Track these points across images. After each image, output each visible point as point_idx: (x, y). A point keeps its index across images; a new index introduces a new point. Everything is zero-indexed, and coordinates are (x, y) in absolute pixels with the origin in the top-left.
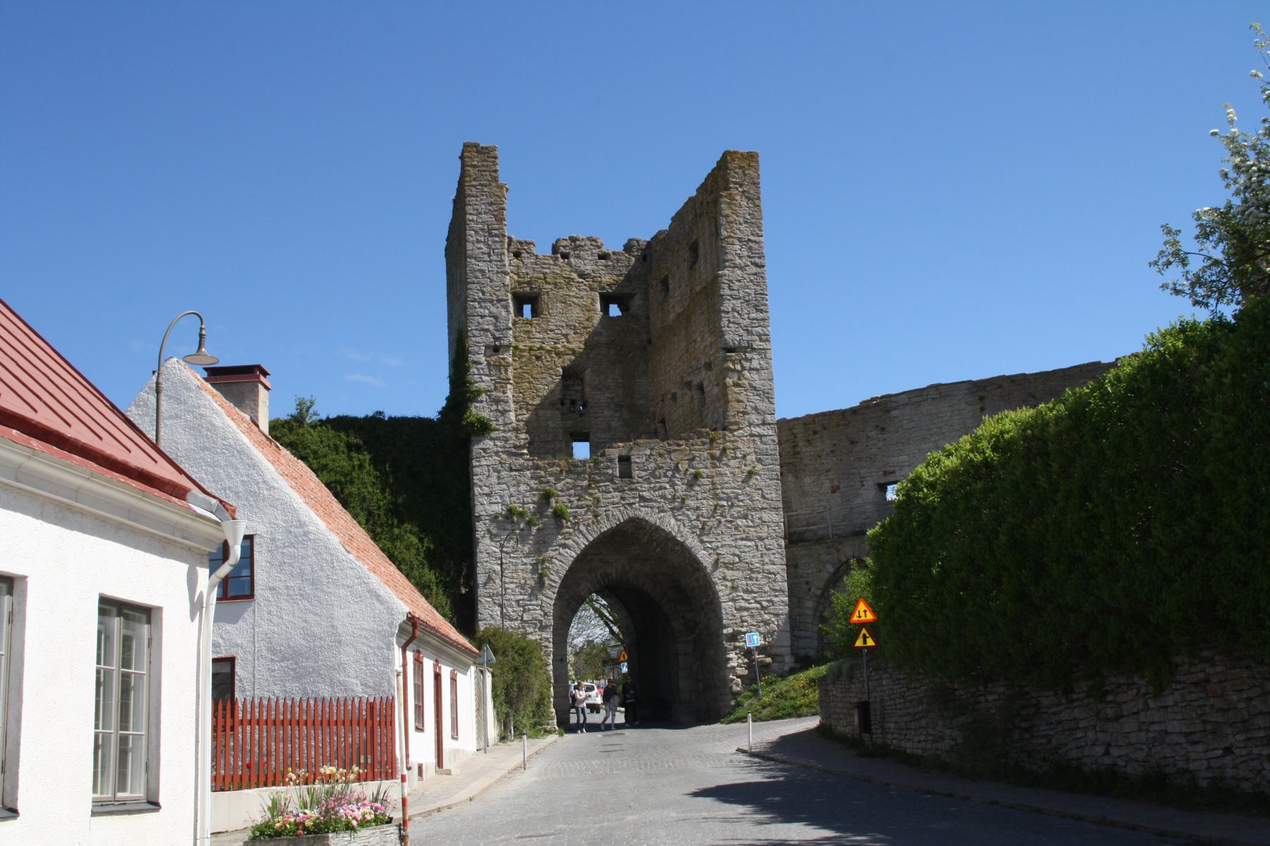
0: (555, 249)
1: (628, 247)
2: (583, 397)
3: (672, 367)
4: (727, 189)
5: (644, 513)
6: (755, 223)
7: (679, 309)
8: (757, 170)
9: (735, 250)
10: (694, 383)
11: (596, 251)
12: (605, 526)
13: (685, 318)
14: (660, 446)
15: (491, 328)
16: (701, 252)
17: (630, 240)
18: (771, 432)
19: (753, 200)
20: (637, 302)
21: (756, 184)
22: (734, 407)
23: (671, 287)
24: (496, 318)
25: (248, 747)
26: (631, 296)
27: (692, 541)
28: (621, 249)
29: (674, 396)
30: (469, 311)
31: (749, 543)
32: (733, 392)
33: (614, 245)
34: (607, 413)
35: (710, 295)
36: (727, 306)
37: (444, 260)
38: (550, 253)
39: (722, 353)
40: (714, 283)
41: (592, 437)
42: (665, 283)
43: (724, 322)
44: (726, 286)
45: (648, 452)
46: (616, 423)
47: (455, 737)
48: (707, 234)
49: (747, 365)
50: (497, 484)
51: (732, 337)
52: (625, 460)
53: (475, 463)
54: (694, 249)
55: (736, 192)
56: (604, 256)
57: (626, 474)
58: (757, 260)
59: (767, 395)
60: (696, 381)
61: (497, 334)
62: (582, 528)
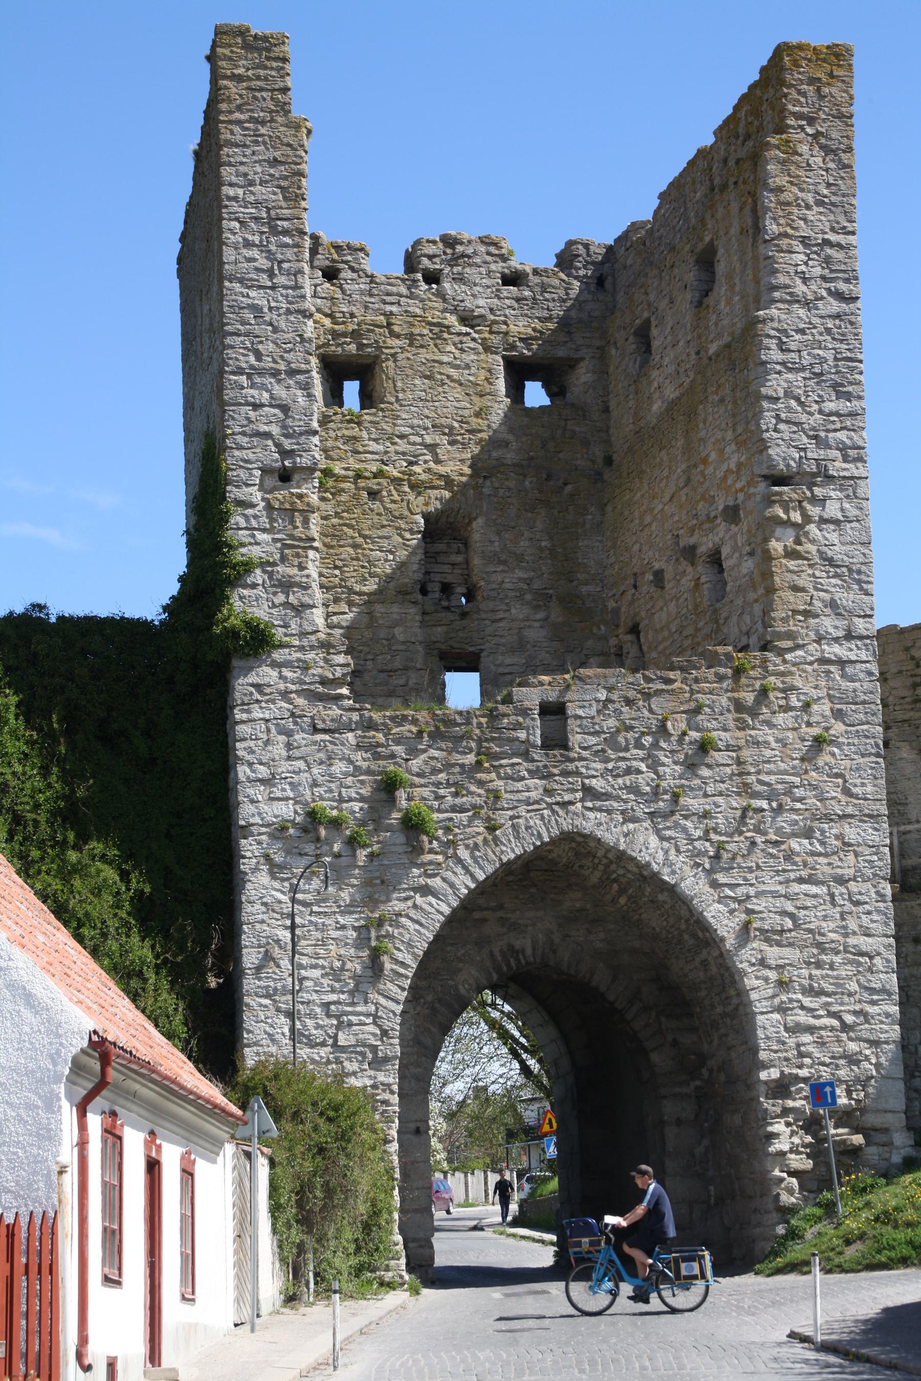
0: (411, 262)
1: (565, 260)
2: (466, 578)
4: (781, 129)
5: (608, 830)
7: (671, 393)
8: (848, 84)
9: (794, 264)
12: (511, 850)
13: (685, 410)
14: (625, 681)
15: (275, 430)
16: (721, 268)
17: (570, 243)
19: (838, 153)
21: (845, 118)
22: (786, 601)
26: (572, 364)
28: (550, 262)
29: (659, 576)
31: (814, 890)
32: (784, 571)
33: (535, 253)
34: (518, 611)
35: (737, 362)
36: (775, 385)
40: (748, 336)
42: (643, 336)
44: (773, 344)
45: (602, 695)
46: (536, 634)
49: (814, 511)
50: (285, 759)
51: (782, 452)
52: (554, 711)
54: (706, 261)
56: (513, 279)
57: (556, 741)
58: (842, 287)
59: (858, 577)
60: (706, 545)
61: (287, 444)
62: (463, 853)
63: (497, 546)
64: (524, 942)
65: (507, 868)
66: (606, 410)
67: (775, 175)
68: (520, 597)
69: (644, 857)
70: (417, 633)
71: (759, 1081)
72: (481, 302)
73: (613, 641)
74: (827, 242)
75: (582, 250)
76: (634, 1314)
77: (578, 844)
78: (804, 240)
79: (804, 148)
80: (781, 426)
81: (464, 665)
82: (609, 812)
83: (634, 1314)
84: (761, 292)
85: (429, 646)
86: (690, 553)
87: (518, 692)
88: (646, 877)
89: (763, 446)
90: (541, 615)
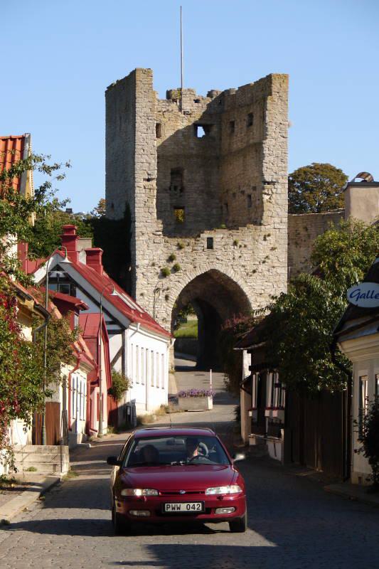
0: (169, 94)
1: (210, 94)
2: (182, 184)
3: (234, 172)
4: (271, 95)
6: (284, 113)
8: (287, 83)
9: (272, 129)
10: (246, 193)
11: (193, 98)
12: (199, 273)
14: (227, 232)
15: (147, 169)
17: (212, 91)
18: (284, 227)
19: (285, 102)
20: (215, 129)
21: (286, 92)
22: (266, 214)
23: (236, 129)
24: (150, 164)
25: (67, 390)
26: (211, 125)
27: (241, 282)
28: (205, 96)
29: (234, 195)
30: (136, 160)
31: (269, 284)
32: (266, 206)
33: (202, 93)
34: (195, 196)
36: (266, 159)
37: (105, 98)
38: (165, 98)
39: (262, 184)
41: (186, 209)
42: (232, 124)
43: (264, 169)
44: (267, 149)
45: (222, 236)
46: (199, 202)
47: (95, 327)
48: (258, 115)
49: (274, 191)
51: (268, 178)
52: (210, 241)
53: (137, 238)
55: (275, 96)
56: (197, 101)
57: (210, 246)
58: (284, 135)
61: (149, 172)
62: (187, 273)
63: (190, 177)
64: (198, 291)
65: (198, 277)
66: (221, 139)
67: (269, 106)
68: (196, 192)
69: (229, 276)
70: (169, 201)
71: (151, 512)
72: (188, 108)
73: (220, 205)
74: (281, 124)
75: (215, 93)
76: (118, 563)
77: (214, 271)
78: (276, 123)
79: (276, 100)
80: (268, 170)
81: (130, 127)
82: (222, 264)
83: (118, 563)
84: (264, 135)
85: (171, 204)
86: (243, 192)
87: (202, 235)
88: (229, 279)
89: (263, 175)
90: (201, 197)
